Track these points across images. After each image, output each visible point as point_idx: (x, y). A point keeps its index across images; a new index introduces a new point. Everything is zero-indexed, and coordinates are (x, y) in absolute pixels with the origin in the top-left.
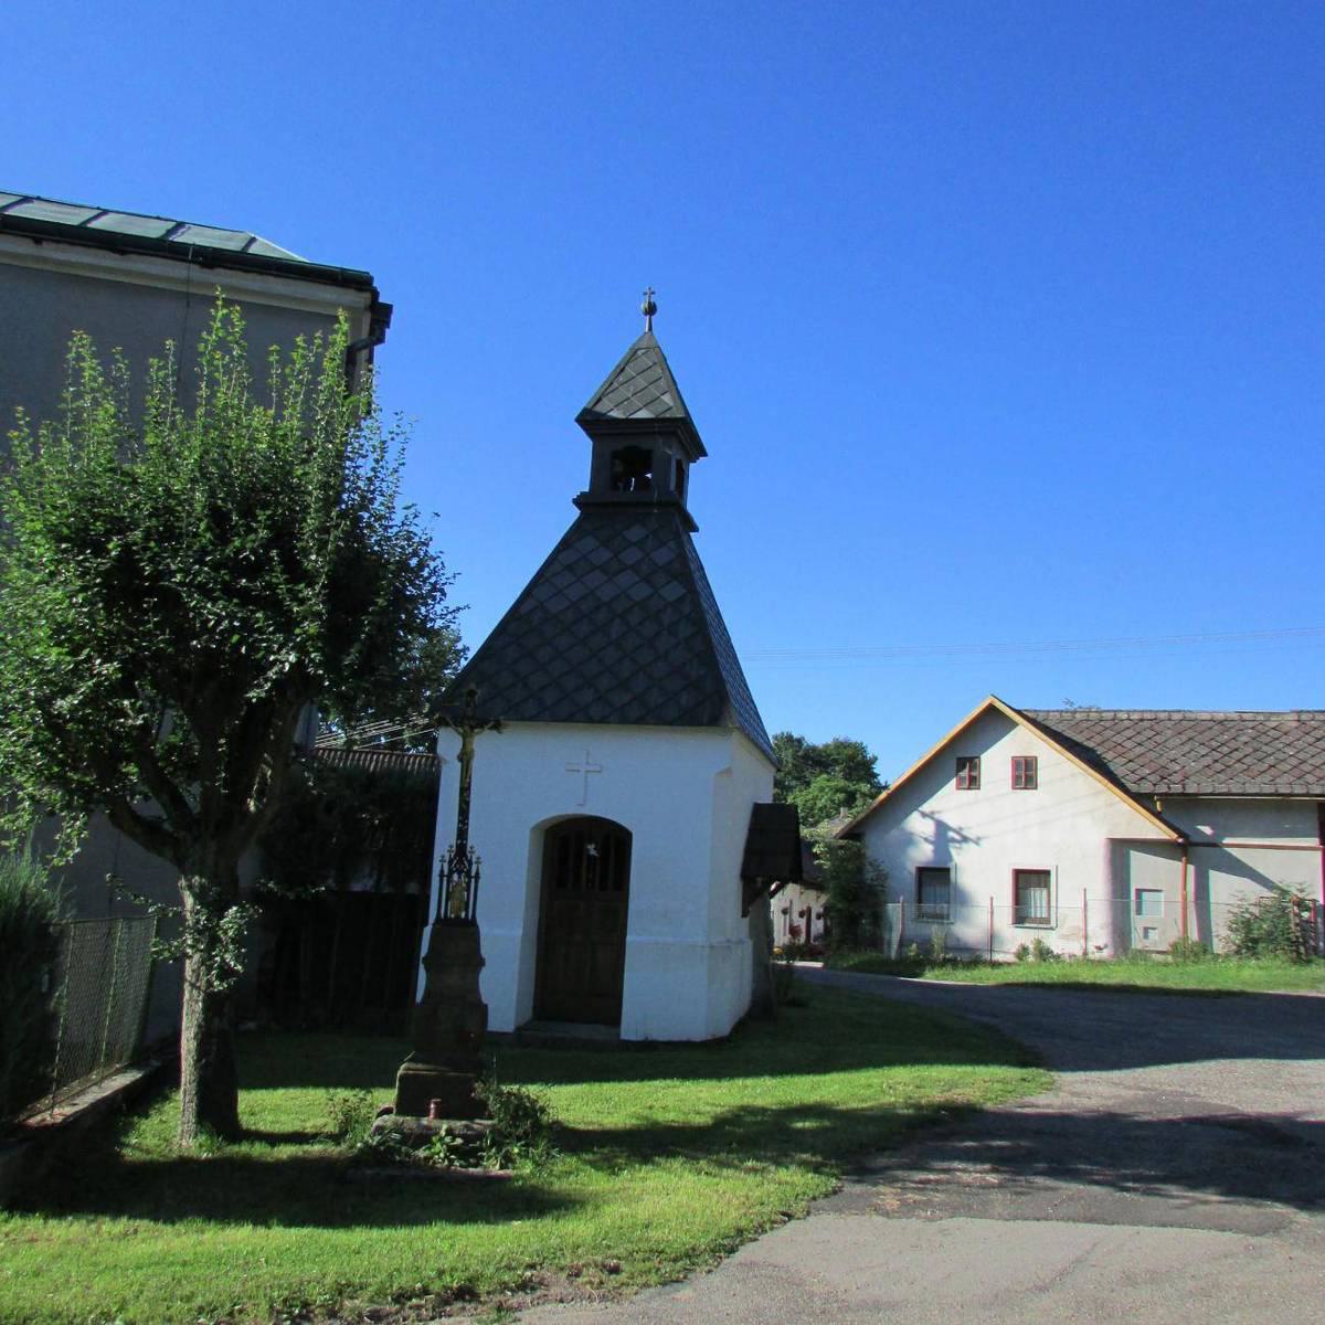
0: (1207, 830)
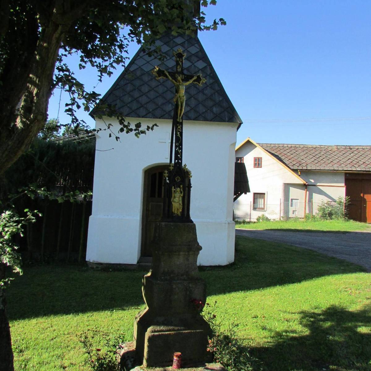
0: (312, 181)
